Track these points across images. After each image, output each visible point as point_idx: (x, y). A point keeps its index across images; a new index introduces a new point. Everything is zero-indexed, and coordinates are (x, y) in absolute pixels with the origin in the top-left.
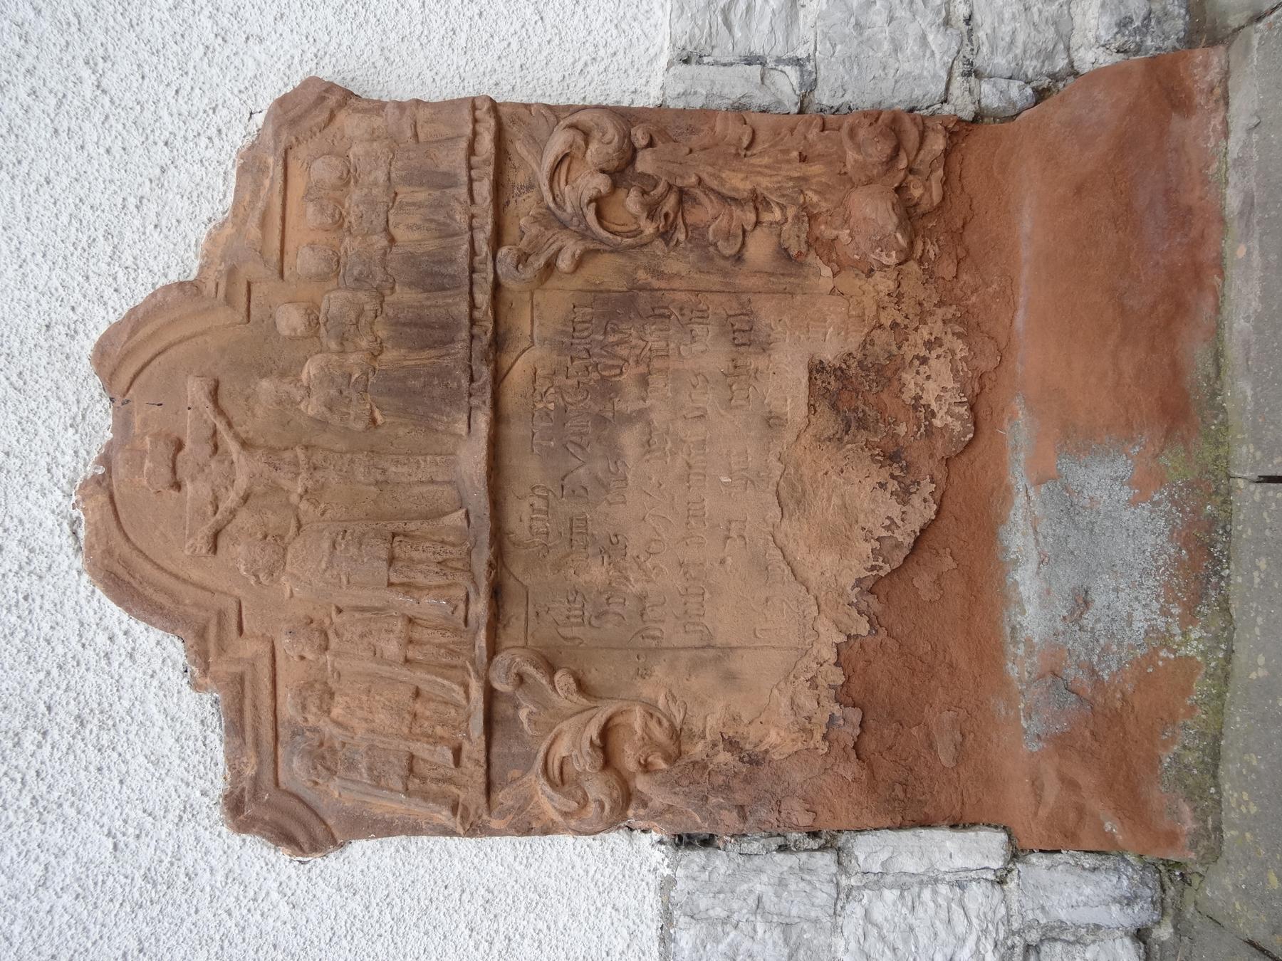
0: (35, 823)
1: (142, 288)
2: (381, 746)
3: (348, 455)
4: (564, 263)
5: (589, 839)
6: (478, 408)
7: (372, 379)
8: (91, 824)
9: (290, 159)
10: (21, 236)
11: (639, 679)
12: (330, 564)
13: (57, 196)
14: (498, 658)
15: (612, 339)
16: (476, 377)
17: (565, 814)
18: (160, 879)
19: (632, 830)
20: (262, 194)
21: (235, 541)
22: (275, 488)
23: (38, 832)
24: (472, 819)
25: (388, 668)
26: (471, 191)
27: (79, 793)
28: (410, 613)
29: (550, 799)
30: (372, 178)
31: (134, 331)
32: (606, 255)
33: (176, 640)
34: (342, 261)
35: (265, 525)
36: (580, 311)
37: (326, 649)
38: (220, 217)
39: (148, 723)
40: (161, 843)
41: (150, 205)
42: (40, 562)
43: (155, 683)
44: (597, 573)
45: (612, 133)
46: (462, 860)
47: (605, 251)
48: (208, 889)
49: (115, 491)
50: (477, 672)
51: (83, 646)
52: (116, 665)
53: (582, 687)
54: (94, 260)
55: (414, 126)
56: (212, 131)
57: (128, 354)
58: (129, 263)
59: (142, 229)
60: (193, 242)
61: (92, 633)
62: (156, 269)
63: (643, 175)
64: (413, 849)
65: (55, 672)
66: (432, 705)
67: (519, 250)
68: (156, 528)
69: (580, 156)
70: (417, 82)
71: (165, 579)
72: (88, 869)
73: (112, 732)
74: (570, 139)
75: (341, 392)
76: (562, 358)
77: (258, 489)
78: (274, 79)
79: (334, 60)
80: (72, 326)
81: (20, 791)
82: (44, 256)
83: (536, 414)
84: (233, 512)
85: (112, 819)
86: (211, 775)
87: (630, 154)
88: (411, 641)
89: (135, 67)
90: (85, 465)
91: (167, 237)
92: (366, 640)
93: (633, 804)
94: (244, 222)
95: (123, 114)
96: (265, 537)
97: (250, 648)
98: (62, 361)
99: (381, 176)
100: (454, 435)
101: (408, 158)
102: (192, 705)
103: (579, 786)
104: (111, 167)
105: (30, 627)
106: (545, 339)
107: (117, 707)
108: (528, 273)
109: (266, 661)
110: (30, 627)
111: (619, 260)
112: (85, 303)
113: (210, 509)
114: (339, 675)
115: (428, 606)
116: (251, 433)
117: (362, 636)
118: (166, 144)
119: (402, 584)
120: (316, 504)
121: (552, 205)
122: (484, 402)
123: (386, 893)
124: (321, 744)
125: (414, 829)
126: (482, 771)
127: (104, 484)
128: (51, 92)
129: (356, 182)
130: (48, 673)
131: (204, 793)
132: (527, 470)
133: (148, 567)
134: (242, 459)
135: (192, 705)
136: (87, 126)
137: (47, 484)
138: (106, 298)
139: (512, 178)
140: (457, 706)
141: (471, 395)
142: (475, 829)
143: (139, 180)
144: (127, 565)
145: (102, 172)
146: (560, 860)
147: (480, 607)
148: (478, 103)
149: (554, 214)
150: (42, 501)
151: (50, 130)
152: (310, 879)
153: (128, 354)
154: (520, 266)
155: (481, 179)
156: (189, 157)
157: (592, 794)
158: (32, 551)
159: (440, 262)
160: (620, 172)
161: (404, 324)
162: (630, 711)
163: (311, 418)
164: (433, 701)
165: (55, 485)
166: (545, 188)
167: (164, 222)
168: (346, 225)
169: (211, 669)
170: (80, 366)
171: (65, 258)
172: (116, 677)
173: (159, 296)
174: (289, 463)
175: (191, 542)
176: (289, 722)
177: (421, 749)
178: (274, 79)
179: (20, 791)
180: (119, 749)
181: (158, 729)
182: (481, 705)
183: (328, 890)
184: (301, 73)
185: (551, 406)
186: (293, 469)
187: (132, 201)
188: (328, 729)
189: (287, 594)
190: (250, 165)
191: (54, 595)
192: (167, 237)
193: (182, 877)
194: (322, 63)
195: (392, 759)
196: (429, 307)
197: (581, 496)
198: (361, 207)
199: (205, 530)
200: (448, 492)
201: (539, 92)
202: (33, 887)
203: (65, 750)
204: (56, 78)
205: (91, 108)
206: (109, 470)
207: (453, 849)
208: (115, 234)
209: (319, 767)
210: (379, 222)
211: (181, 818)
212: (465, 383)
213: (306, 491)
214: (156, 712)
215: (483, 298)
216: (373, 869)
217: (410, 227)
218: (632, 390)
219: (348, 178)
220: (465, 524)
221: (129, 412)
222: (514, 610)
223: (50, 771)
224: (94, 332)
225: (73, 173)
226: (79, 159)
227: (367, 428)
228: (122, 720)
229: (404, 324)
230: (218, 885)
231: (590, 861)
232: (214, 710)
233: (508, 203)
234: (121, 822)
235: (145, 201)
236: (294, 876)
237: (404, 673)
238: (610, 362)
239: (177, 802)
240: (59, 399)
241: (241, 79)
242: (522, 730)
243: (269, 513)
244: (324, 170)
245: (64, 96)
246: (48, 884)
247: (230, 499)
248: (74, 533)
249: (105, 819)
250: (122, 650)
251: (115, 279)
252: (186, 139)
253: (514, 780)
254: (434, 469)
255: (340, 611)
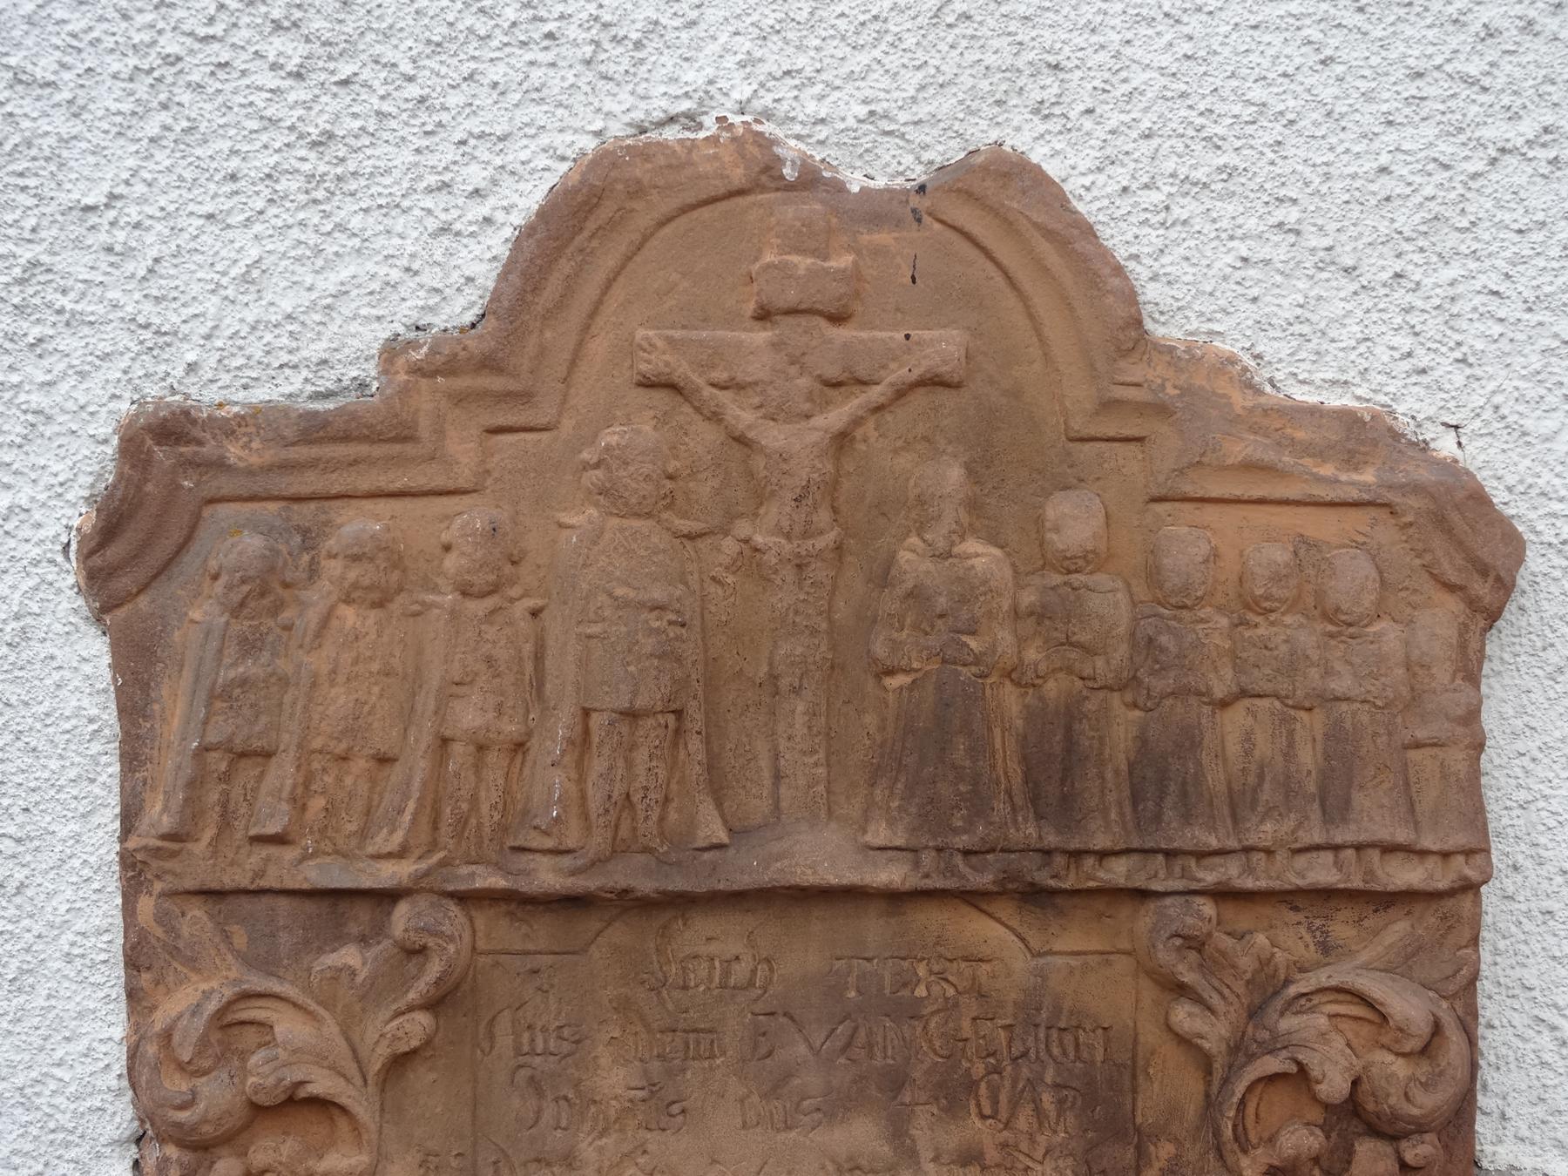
0: (133, 61)
1: (1129, 237)
2: (287, 699)
3: (824, 625)
4: (1184, 1016)
5: (120, 1067)
6: (917, 864)
7: (966, 672)
8: (131, 162)
9: (1373, 512)
10: (1223, 15)
11: (419, 1157)
12: (622, 604)
13: (1299, 77)
14: (454, 909)
15: (1047, 1099)
16: (974, 859)
17: (167, 1036)
18: (31, 291)
19: (138, 1141)
20: (1308, 461)
21: (661, 421)
22: (761, 495)
23: (116, 67)
24: (155, 864)
25: (432, 705)
26: (1318, 848)
27: (189, 139)
28: (534, 743)
29: (196, 1010)
30: (1338, 666)
31: (1049, 234)
32: (1201, 1087)
33: (477, 310)
34: (1185, 613)
35: (693, 474)
36: (1097, 1040)
37: (464, 594)
38: (1261, 376)
39: (320, 262)
40: (98, 291)
41: (1284, 248)
42: (617, 59)
43: (395, 275)
44: (614, 1079)
45: (1426, 1102)
46: (77, 838)
47: (1209, 1084)
48: (15, 378)
49: (750, 199)
50: (427, 874)
51: (463, 143)
52: (428, 202)
53: (400, 1063)
54: (1180, 148)
55: (1434, 750)
56: (1423, 360)
57: (1007, 223)
58: (1177, 212)
59: (1239, 232)
60: (1216, 327)
61: (486, 156)
62: (1165, 260)
63: (1350, 1152)
64: (96, 747)
65: (413, 91)
66: (363, 788)
67: (1210, 935)
68: (684, 275)
69: (1385, 1040)
70: (1519, 723)
71: (588, 292)
72: (47, 159)
73: (303, 198)
74: (1413, 1030)
75: (941, 616)
76: (1010, 1009)
77: (759, 463)
78: (1521, 468)
79: (1557, 573)
80: (1057, 110)
81: (191, 34)
82: (1187, 57)
83: (906, 964)
84: (715, 417)
85: (142, 200)
86: (226, 378)
87: (1390, 1131)
88: (481, 748)
89: (1540, 216)
90: (798, 137)
91: (1225, 278)
92: (483, 667)
93: (188, 1157)
94: (1254, 429)
95: (1453, 195)
96: (671, 477)
97: (463, 451)
98: (992, 93)
99: (1342, 684)
100: (866, 817)
101: (1375, 734)
102: (356, 343)
103: (220, 1059)
104: (1354, 176)
105: (495, 43)
106: (1044, 978)
107: (351, 205)
108: (1165, 956)
109: (440, 482)
110: (495, 43)
111: (1192, 1110)
112: (1100, 133)
113: (720, 375)
114: (416, 614)
115: (549, 781)
116: (863, 447)
117: (489, 661)
118: (1398, 276)
119: (586, 731)
120: (732, 567)
121: (1292, 990)
122: (927, 876)
123: (13, 699)
124: (286, 585)
125: (133, 755)
126: (245, 882)
127: (764, 178)
128: (1492, 64)
129: (1332, 636)
130: (410, 79)
131: (192, 368)
132: (804, 953)
133: (610, 262)
134: (815, 437)
135: (356, 343)
136: (1430, 131)
137: (762, 69)
138: (1110, 170)
139: (1341, 916)
140: (364, 834)
141: (939, 850)
142: (135, 871)
143: (1332, 227)
144: (612, 225)
145: (1345, 158)
146: (80, 1015)
147: (547, 877)
148: (1479, 859)
149: (1276, 993)
150: (730, 62)
151: (1422, 65)
152: (35, 563)
153: (1007, 223)
154: (1178, 941)
155: (1338, 865)
156: (1375, 316)
157: (206, 1086)
158: (638, 45)
159: (1184, 794)
160: (1356, 1115)
161: (1069, 729)
162: (360, 1145)
163: (892, 557)
164: (371, 790)
165: (762, 85)
166: (1322, 978)
167: (1252, 272)
168: (1250, 616)
169: (424, 382)
170: (983, 124)
171: (1184, 95)
172: (406, 204)
173: (1115, 282)
174: (809, 523)
175: (660, 344)
176: (327, 523)
177: (283, 773)
178: (1521, 468)
179: (191, 34)
180: (273, 211)
181: (309, 280)
182: (366, 883)
183: (17, 596)
184: (1532, 515)
185: (921, 991)
186: (798, 529)
187: (1291, 215)
188: (318, 597)
189: (566, 518)
190: (1363, 435)
191: (555, 87)
192: (1225, 278)
193: (36, 332)
194: (1551, 553)
195: (264, 719)
196: (1101, 776)
197: (755, 1047)
198: (1284, 648)
199: (682, 369)
200: (757, 806)
201: (1502, 944)
202: (12, 61)
203: (268, 113)
204: (1518, 73)
205: (1463, 138)
206: (791, 187)
207: (95, 820)
208: (1231, 186)
209: (246, 588)
210: (1258, 679)
211: (146, 326)
212: (962, 841)
213: (757, 550)
214: (338, 275)
215: (1118, 872)
216: (56, 676)
217: (1248, 737)
218: (953, 1137)
219: (1339, 623)
220: (700, 843)
221: (899, 224)
222: (543, 931)
223: (228, 87)
224: (1046, 150)
225: (1341, 108)
226: (1368, 118)
227: (876, 661)
228: (326, 215)
229: (1069, 729)
230: (22, 397)
231: (79, 1069)
232: (346, 383)
233: (1296, 909)
234: (135, 218)
235: (1292, 238)
236: (42, 534)
237: (422, 738)
238: (1003, 1098)
239: (175, 319)
240: (922, 88)
241: (1520, 408)
242: (320, 951)
243: (716, 483)
244: (1352, 579)
245: (1485, 89)
246: (19, 88)
247: (741, 415)
248: (672, 120)
249: (140, 188)
250: (455, 213)
251: (1146, 186)
252: (1408, 310)
253: (227, 937)
254: (802, 782)
255: (535, 613)
